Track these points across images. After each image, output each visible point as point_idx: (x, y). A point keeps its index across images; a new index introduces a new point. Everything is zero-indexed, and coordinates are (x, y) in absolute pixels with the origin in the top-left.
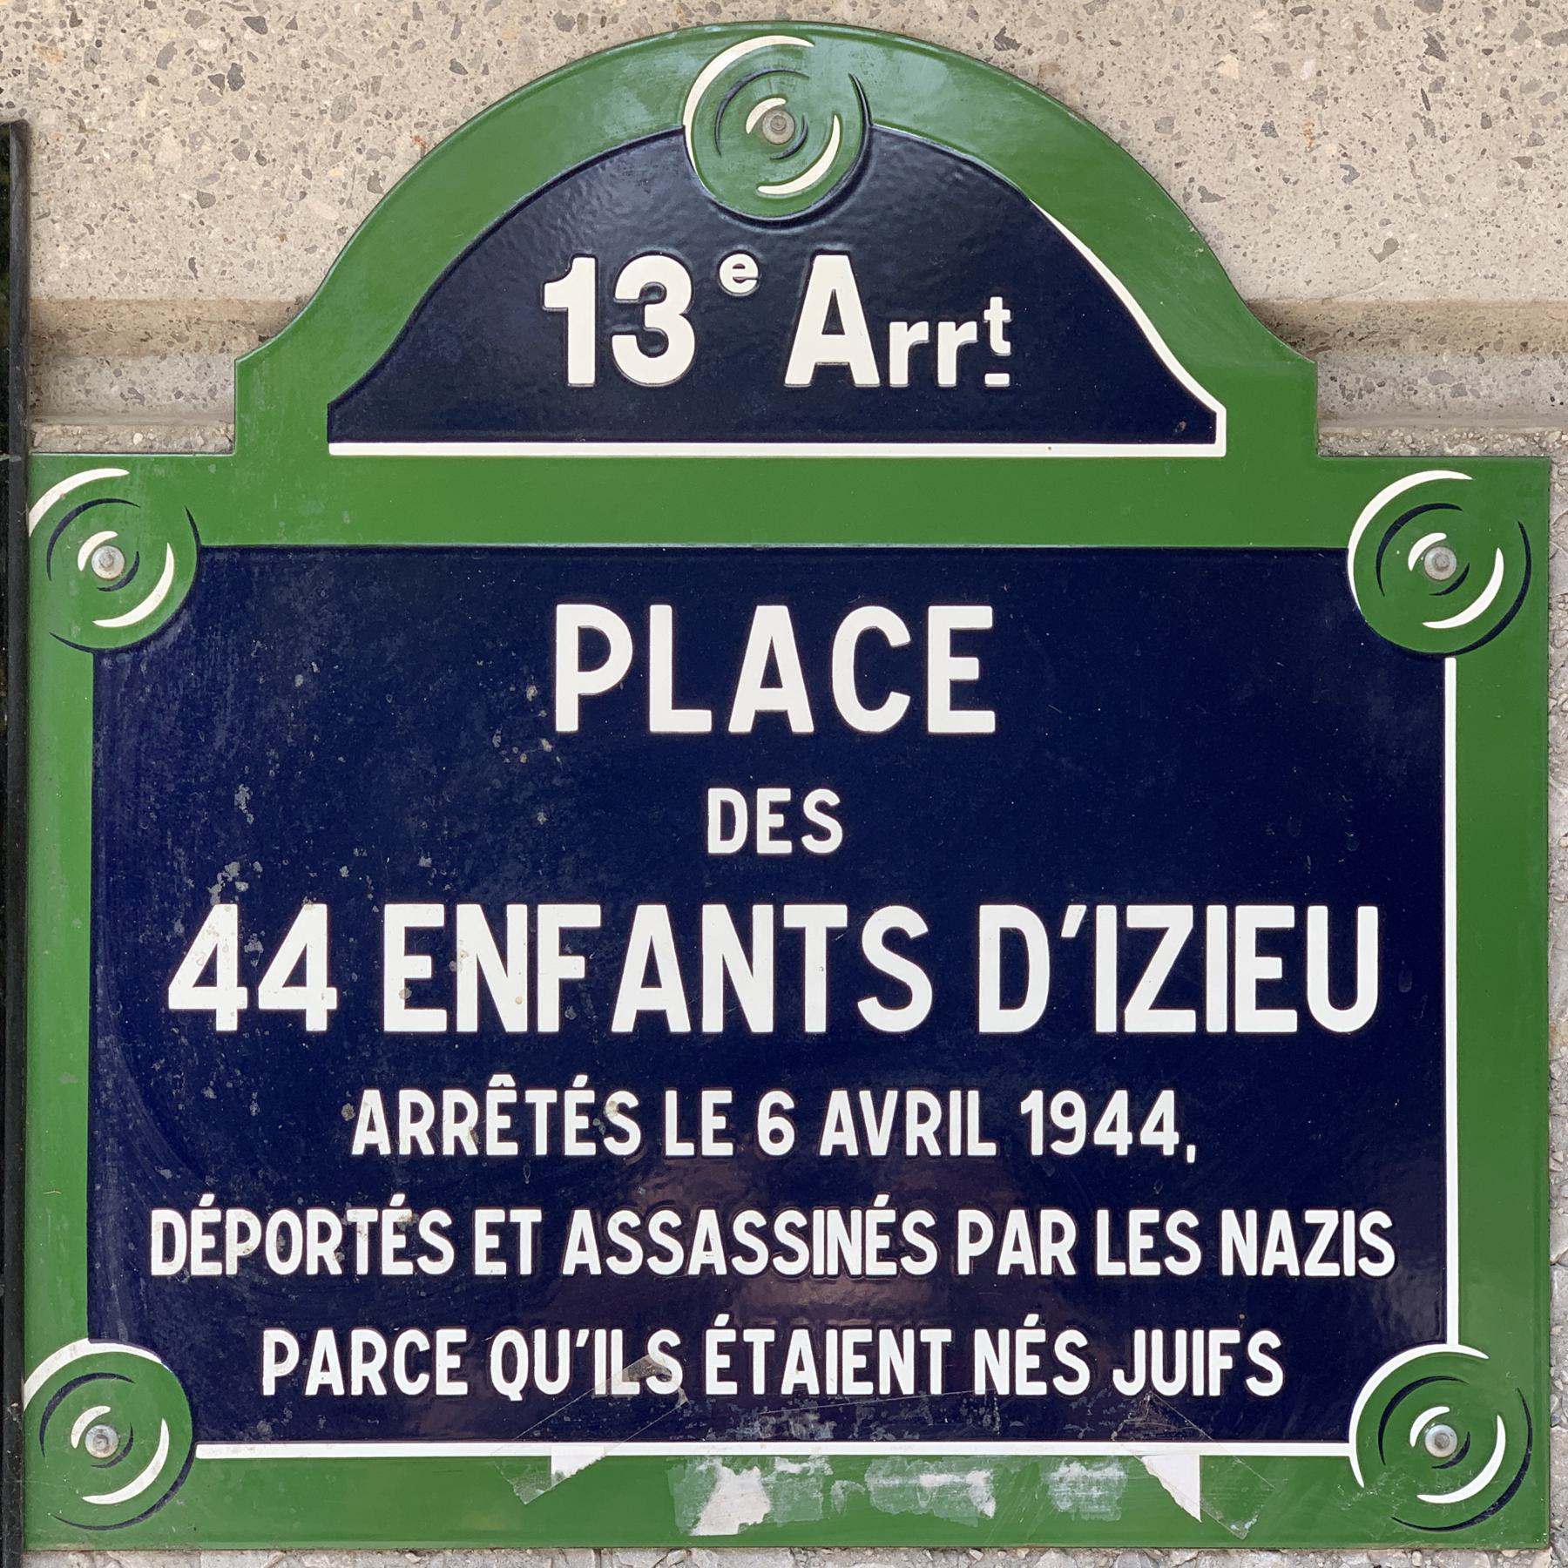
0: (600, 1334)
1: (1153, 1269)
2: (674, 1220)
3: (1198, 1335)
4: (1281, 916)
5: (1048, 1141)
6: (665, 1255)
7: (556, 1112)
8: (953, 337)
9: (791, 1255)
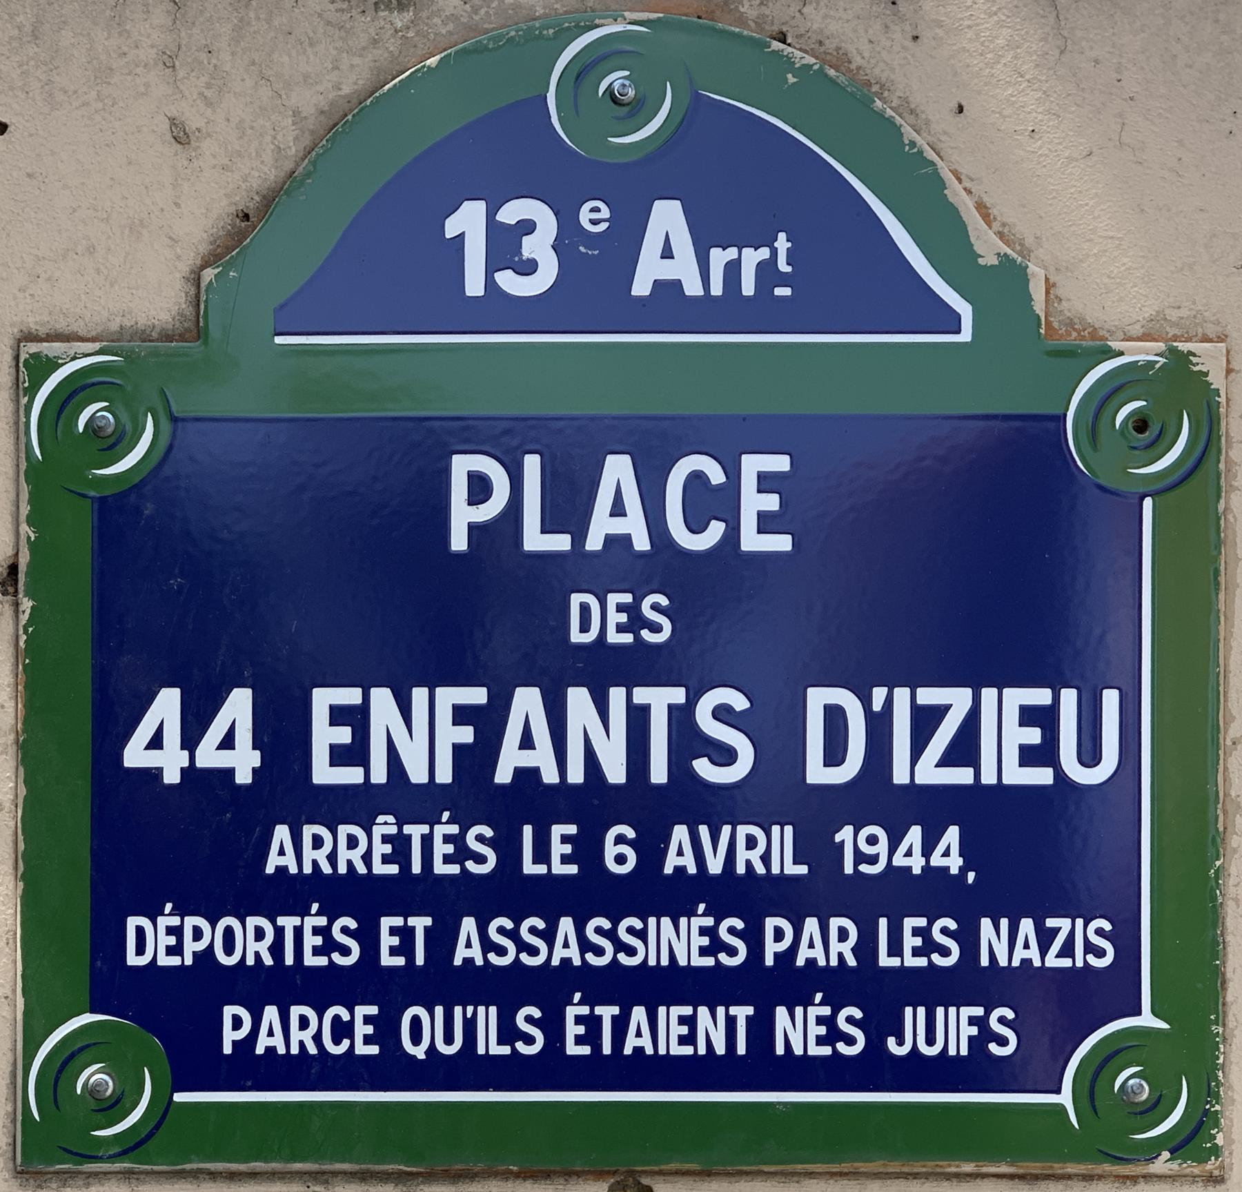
0: (481, 1009)
1: (922, 962)
2: (540, 924)
3: (952, 1010)
4: (1042, 697)
5: (856, 864)
6: (534, 951)
7: (427, 841)
8: (752, 258)
9: (631, 952)
